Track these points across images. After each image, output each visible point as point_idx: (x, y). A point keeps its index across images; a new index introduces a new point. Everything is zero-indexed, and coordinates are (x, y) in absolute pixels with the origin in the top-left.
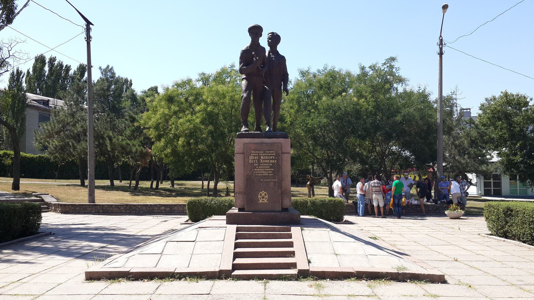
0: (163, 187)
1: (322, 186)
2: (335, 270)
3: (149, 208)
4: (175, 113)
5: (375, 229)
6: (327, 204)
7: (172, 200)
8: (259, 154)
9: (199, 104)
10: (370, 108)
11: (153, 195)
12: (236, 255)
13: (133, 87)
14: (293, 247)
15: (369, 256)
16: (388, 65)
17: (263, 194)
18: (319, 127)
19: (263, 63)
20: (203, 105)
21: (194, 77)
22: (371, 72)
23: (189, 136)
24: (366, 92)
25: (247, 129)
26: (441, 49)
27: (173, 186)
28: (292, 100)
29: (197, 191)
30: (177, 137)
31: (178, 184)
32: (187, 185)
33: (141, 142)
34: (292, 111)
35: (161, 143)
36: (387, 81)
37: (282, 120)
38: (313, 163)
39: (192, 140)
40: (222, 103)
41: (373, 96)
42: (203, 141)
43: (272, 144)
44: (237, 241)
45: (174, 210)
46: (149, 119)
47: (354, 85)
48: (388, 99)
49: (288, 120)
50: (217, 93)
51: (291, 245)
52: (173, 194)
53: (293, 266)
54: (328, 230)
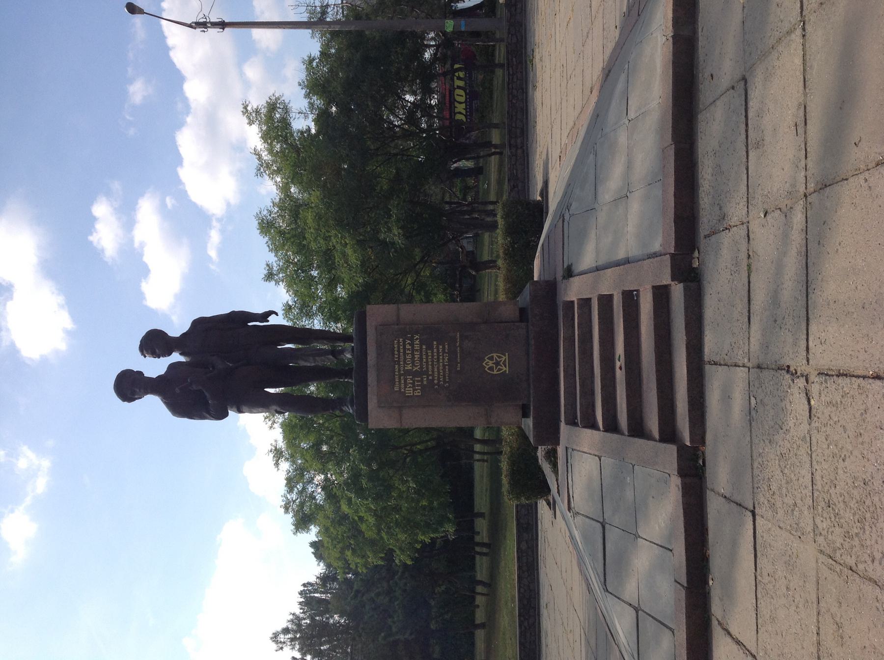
8: (400, 375)
17: (491, 363)
26: (215, 25)
43: (379, 347)
51: (606, 301)
53: (661, 295)
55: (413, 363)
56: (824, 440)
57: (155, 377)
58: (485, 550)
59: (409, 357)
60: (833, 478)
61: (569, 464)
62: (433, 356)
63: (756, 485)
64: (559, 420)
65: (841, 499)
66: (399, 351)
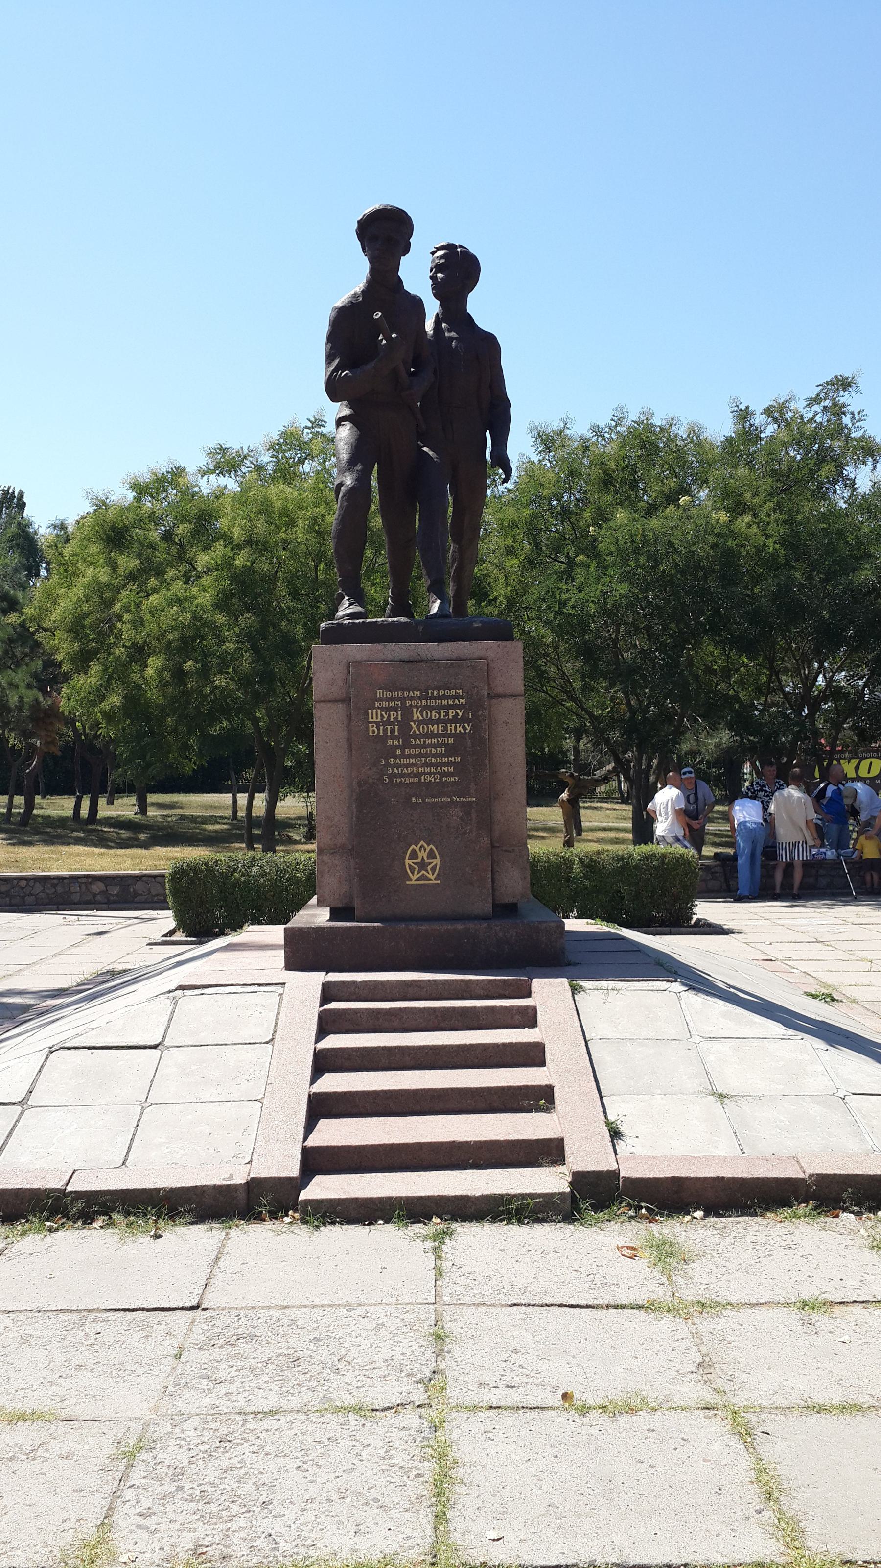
0: (113, 814)
1: (602, 800)
2: (727, 1173)
3: (54, 886)
4: (132, 577)
5: (806, 951)
6: (637, 867)
7: (133, 858)
8: (403, 700)
9: (206, 548)
10: (772, 545)
11: (78, 841)
12: (321, 1107)
13: (27, 512)
14: (542, 1063)
15: (853, 1101)
16: (827, 403)
17: (423, 854)
18: (605, 612)
19: (417, 361)
20: (219, 550)
21: (194, 461)
22: (770, 430)
23: (179, 650)
24: (754, 496)
25: (359, 609)
27: (143, 810)
28: (513, 525)
29: (217, 827)
30: (139, 653)
31: (160, 806)
32: (189, 806)
33: (35, 676)
34: (512, 563)
35: (90, 679)
36: (823, 456)
37: (482, 595)
38: (578, 734)
39: (190, 663)
40: (286, 543)
41: (778, 507)
42: (225, 662)
43: (456, 662)
44: (322, 1045)
45: (136, 894)
46: (54, 603)
47: (714, 474)
48: (824, 517)
49: (501, 592)
50: (265, 508)
52: (142, 837)
53: (549, 1152)
54: (677, 987)
55: (423, 722)
56: (328, 1435)
57: (401, 274)
58: (84, 812)
59: (434, 715)
60: (267, 1449)
61: (256, 988)
62: (436, 755)
63: (242, 1312)
64: (328, 969)
65: (235, 1461)
66: (444, 697)
